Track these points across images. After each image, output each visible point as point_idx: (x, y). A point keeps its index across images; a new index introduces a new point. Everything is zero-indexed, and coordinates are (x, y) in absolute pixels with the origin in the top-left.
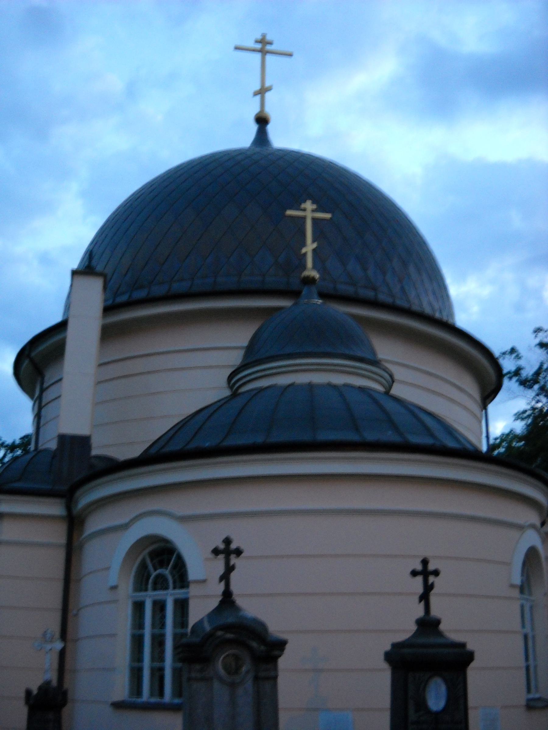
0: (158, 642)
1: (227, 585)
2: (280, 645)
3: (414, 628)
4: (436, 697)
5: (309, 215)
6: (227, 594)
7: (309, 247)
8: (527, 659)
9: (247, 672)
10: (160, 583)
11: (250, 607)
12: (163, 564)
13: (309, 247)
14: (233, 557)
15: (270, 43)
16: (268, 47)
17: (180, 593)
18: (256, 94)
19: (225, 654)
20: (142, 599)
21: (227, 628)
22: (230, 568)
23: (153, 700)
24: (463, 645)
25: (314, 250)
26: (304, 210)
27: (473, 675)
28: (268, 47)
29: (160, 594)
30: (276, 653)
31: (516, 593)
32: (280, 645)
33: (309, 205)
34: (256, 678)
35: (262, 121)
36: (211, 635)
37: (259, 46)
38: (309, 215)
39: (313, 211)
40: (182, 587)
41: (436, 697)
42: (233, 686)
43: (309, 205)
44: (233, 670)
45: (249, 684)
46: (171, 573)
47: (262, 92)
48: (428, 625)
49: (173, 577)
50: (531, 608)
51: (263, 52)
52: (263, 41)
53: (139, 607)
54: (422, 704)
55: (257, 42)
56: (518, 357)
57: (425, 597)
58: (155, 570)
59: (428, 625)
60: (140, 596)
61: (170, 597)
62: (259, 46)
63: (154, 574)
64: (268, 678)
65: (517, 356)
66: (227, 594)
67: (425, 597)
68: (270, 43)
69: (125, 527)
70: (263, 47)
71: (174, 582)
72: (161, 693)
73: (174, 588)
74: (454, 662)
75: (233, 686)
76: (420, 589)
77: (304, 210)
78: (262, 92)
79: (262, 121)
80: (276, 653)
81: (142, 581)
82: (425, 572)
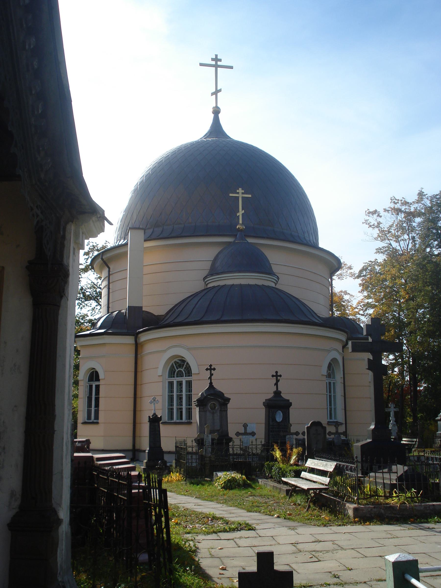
0: (180, 398)
1: (211, 381)
2: (228, 400)
3: (371, 373)
4: (279, 417)
5: (240, 196)
6: (211, 383)
7: (241, 213)
8: (330, 405)
9: (218, 409)
10: (180, 374)
11: (218, 386)
12: (180, 366)
13: (241, 213)
14: (212, 371)
15: (220, 60)
16: (219, 63)
17: (189, 378)
18: (212, 94)
19: (392, 419)
20: (172, 380)
21: (211, 395)
22: (211, 375)
23: (178, 421)
24: (289, 400)
25: (242, 214)
26: (238, 193)
27: (291, 410)
28: (219, 63)
29: (179, 379)
30: (227, 402)
31: (324, 378)
32: (228, 400)
33: (240, 190)
34: (221, 411)
35: (216, 111)
36: (206, 397)
37: (214, 63)
38: (240, 196)
39: (243, 193)
40: (189, 376)
41: (279, 417)
42: (213, 413)
43: (240, 190)
44: (213, 408)
45: (218, 413)
46: (184, 370)
47: (216, 92)
48: (277, 393)
49: (185, 371)
50: (334, 383)
51: (216, 66)
52: (216, 59)
53: (171, 384)
54: (274, 420)
55: (213, 60)
56: (379, 216)
57: (276, 384)
58: (177, 369)
59: (277, 393)
60: (171, 379)
61: (184, 380)
62: (214, 63)
63: (177, 370)
64: (224, 411)
65: (379, 214)
66: (211, 383)
67: (276, 384)
68: (220, 60)
69: (165, 351)
70: (216, 63)
71: (186, 374)
72: (181, 419)
73: (186, 376)
74: (285, 406)
75: (213, 413)
76: (275, 382)
77: (238, 193)
78: (216, 92)
79: (216, 111)
80: (227, 402)
81: (172, 373)
82: (277, 376)
